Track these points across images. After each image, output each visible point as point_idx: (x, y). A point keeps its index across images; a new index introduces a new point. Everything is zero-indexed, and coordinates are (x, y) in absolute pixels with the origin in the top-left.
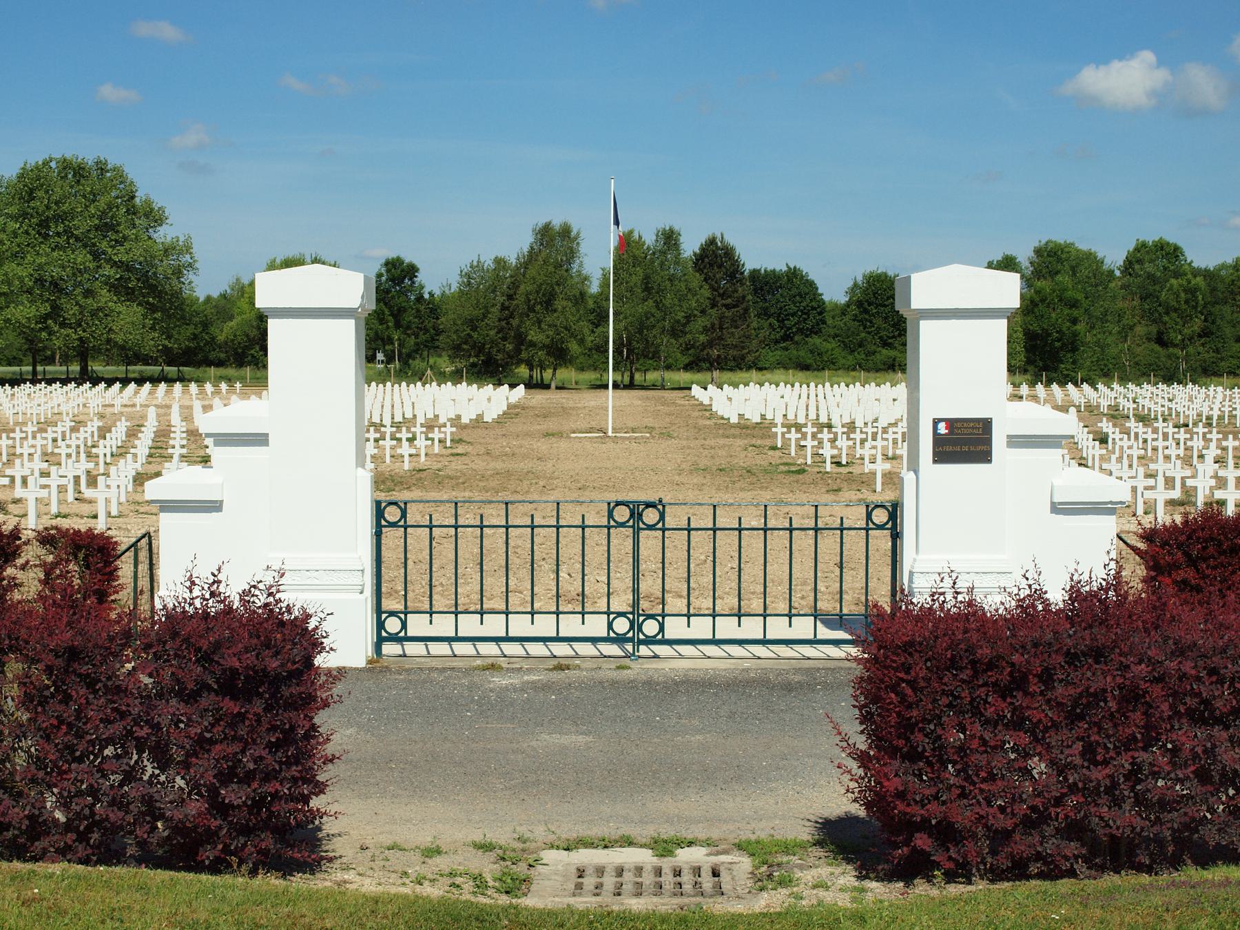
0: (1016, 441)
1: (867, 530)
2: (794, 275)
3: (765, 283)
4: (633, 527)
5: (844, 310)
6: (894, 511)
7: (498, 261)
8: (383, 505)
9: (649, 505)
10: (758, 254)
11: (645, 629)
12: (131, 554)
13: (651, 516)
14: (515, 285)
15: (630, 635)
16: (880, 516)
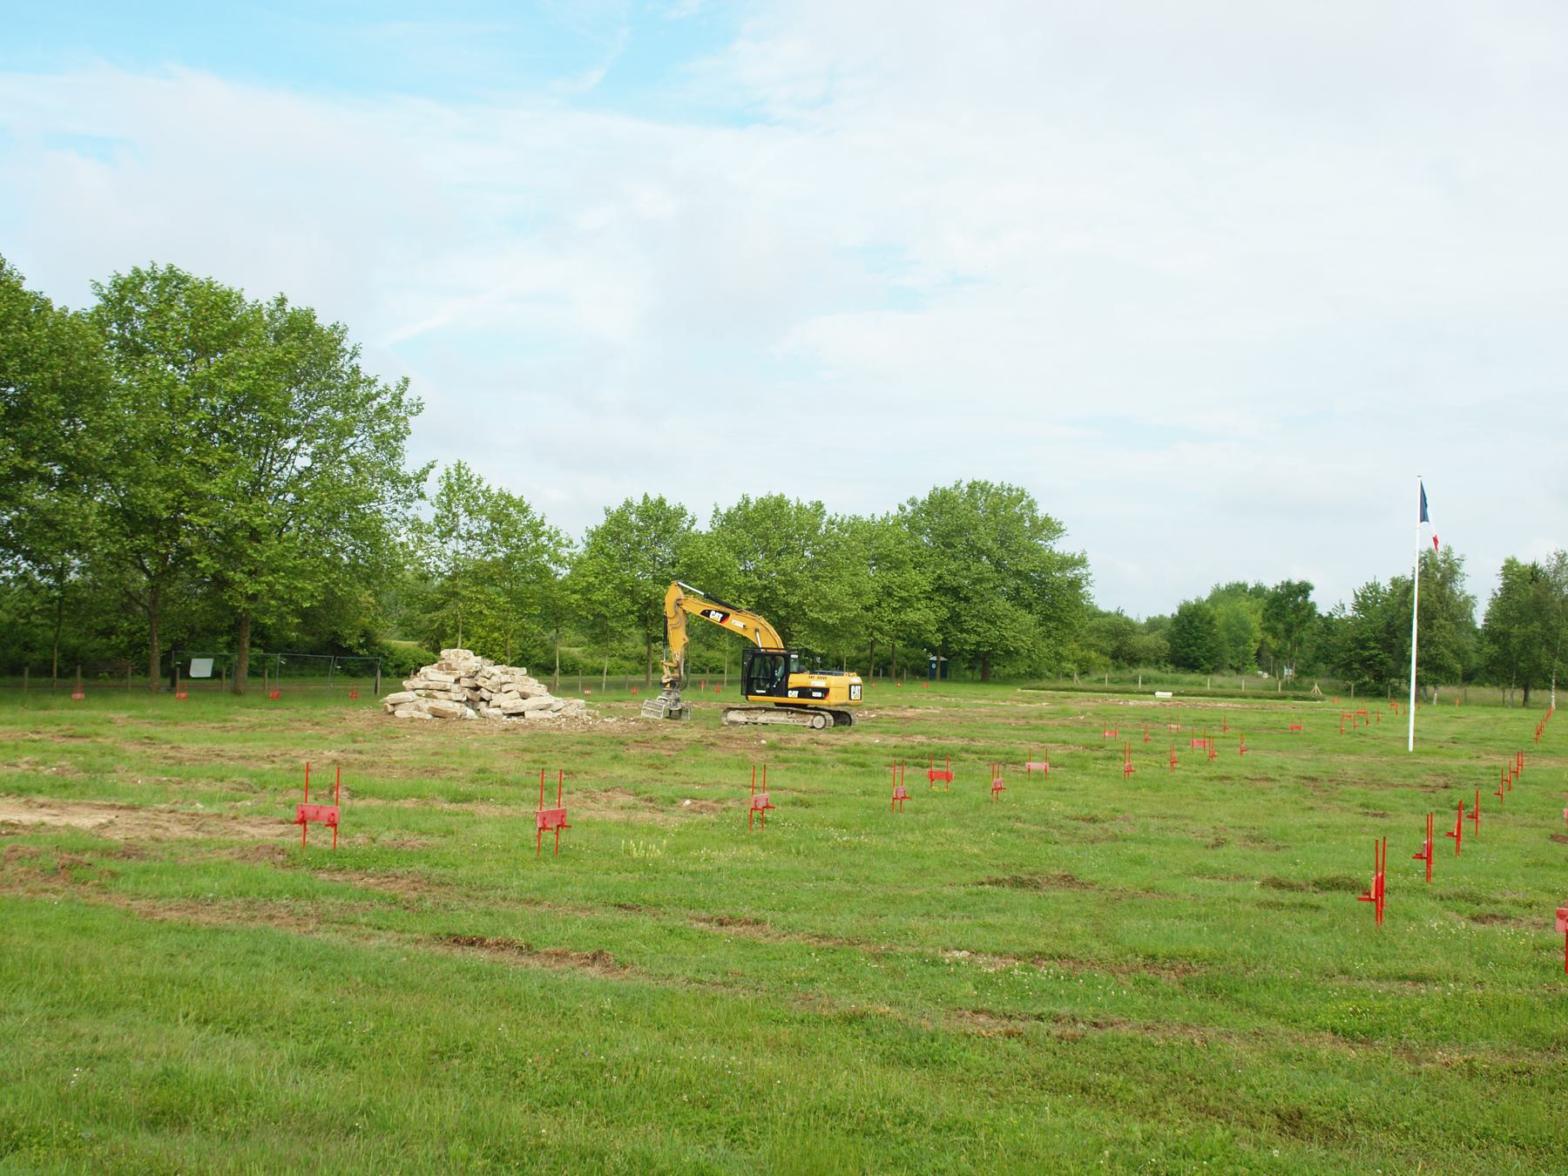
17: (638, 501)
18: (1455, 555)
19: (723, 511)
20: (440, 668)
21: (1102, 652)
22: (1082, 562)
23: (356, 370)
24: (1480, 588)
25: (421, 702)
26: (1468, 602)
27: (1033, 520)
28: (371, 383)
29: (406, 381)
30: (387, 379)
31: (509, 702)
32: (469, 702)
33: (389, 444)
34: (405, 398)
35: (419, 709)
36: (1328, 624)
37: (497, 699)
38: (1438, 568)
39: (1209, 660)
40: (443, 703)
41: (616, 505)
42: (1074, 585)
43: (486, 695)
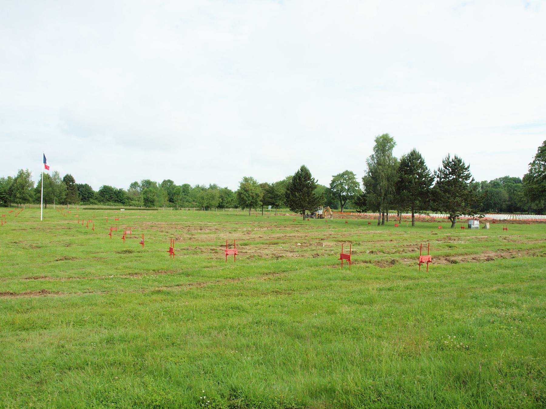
3: (80, 187)
7: (9, 177)
10: (79, 181)
14: (13, 185)
18: (29, 171)
24: (35, 179)
26: (33, 183)
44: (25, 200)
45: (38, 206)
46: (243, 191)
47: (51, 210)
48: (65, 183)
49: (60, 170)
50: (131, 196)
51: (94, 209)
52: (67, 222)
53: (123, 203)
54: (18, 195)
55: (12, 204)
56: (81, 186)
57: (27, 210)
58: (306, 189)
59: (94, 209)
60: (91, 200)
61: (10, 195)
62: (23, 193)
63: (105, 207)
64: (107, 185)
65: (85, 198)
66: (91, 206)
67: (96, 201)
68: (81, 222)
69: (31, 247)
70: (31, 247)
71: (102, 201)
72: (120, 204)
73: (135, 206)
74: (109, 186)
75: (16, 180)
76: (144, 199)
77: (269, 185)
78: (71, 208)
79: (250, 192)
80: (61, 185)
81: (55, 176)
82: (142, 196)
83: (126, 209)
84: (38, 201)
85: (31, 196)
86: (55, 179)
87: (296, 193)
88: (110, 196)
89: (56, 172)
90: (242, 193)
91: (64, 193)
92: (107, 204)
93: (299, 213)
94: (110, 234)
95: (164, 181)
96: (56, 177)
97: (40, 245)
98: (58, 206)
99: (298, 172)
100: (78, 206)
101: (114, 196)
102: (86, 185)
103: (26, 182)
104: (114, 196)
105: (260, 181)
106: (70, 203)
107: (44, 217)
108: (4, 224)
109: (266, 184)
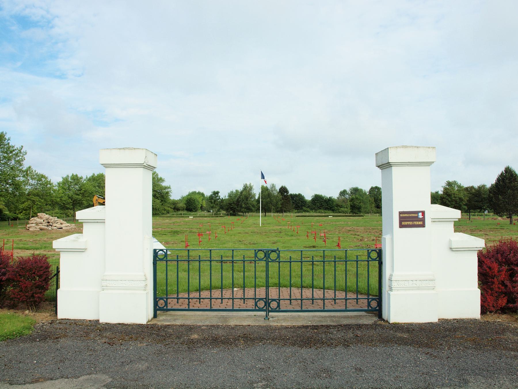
0: (434, 221)
1: (368, 261)
2: (300, 195)
3: (293, 196)
4: (265, 260)
5: (310, 202)
6: (380, 253)
7: (236, 191)
8: (157, 251)
9: (273, 251)
10: (292, 191)
11: (271, 305)
12: (55, 277)
13: (273, 256)
14: (240, 197)
15: (265, 308)
16: (374, 255)
17: (70, 175)
18: (252, 185)
19: (88, 177)
20: (39, 218)
21: (171, 208)
22: (169, 188)
23: (9, 143)
24: (257, 192)
25: (36, 226)
26: (254, 195)
27: (158, 178)
28: (13, 147)
29: (22, 147)
30: (17, 146)
31: (59, 225)
32: (47, 226)
33: (19, 162)
34: (22, 151)
35: (36, 228)
36: (222, 200)
37: (55, 225)
38: (248, 187)
39: (194, 209)
40: (41, 226)
41: (65, 176)
42: (167, 193)
43: (51, 224)
44: (249, 210)
45: (257, 214)
46: (445, 196)
47: (270, 218)
48: (280, 194)
49: (275, 182)
50: (340, 204)
51: (305, 216)
52: (280, 227)
53: (333, 211)
54: (243, 206)
55: (239, 213)
56: (296, 196)
57: (251, 218)
58: (511, 192)
59: (305, 216)
60: (304, 208)
61: (238, 205)
62: (247, 204)
63: (320, 214)
64: (318, 194)
65: (299, 207)
66: (304, 214)
67: (308, 209)
68: (290, 228)
69: (250, 243)
70: (250, 243)
71: (314, 209)
72: (330, 211)
73: (343, 212)
74: (320, 194)
75: (242, 192)
76: (351, 206)
77: (475, 189)
78: (286, 216)
79: (453, 196)
80: (277, 196)
81: (272, 188)
82: (349, 203)
83: (333, 216)
84: (258, 210)
85: (253, 206)
86: (272, 191)
87: (500, 196)
88: (321, 204)
89: (273, 185)
90: (444, 198)
91: (280, 203)
92: (318, 211)
93: (505, 217)
94: (307, 236)
95: (372, 188)
96: (273, 189)
97: (256, 242)
98: (276, 214)
99: (502, 174)
100: (292, 214)
101: (324, 204)
102: (299, 194)
103: (250, 194)
104: (324, 204)
105: (466, 183)
106: (285, 212)
107: (263, 224)
108: (233, 229)
109: (472, 187)
